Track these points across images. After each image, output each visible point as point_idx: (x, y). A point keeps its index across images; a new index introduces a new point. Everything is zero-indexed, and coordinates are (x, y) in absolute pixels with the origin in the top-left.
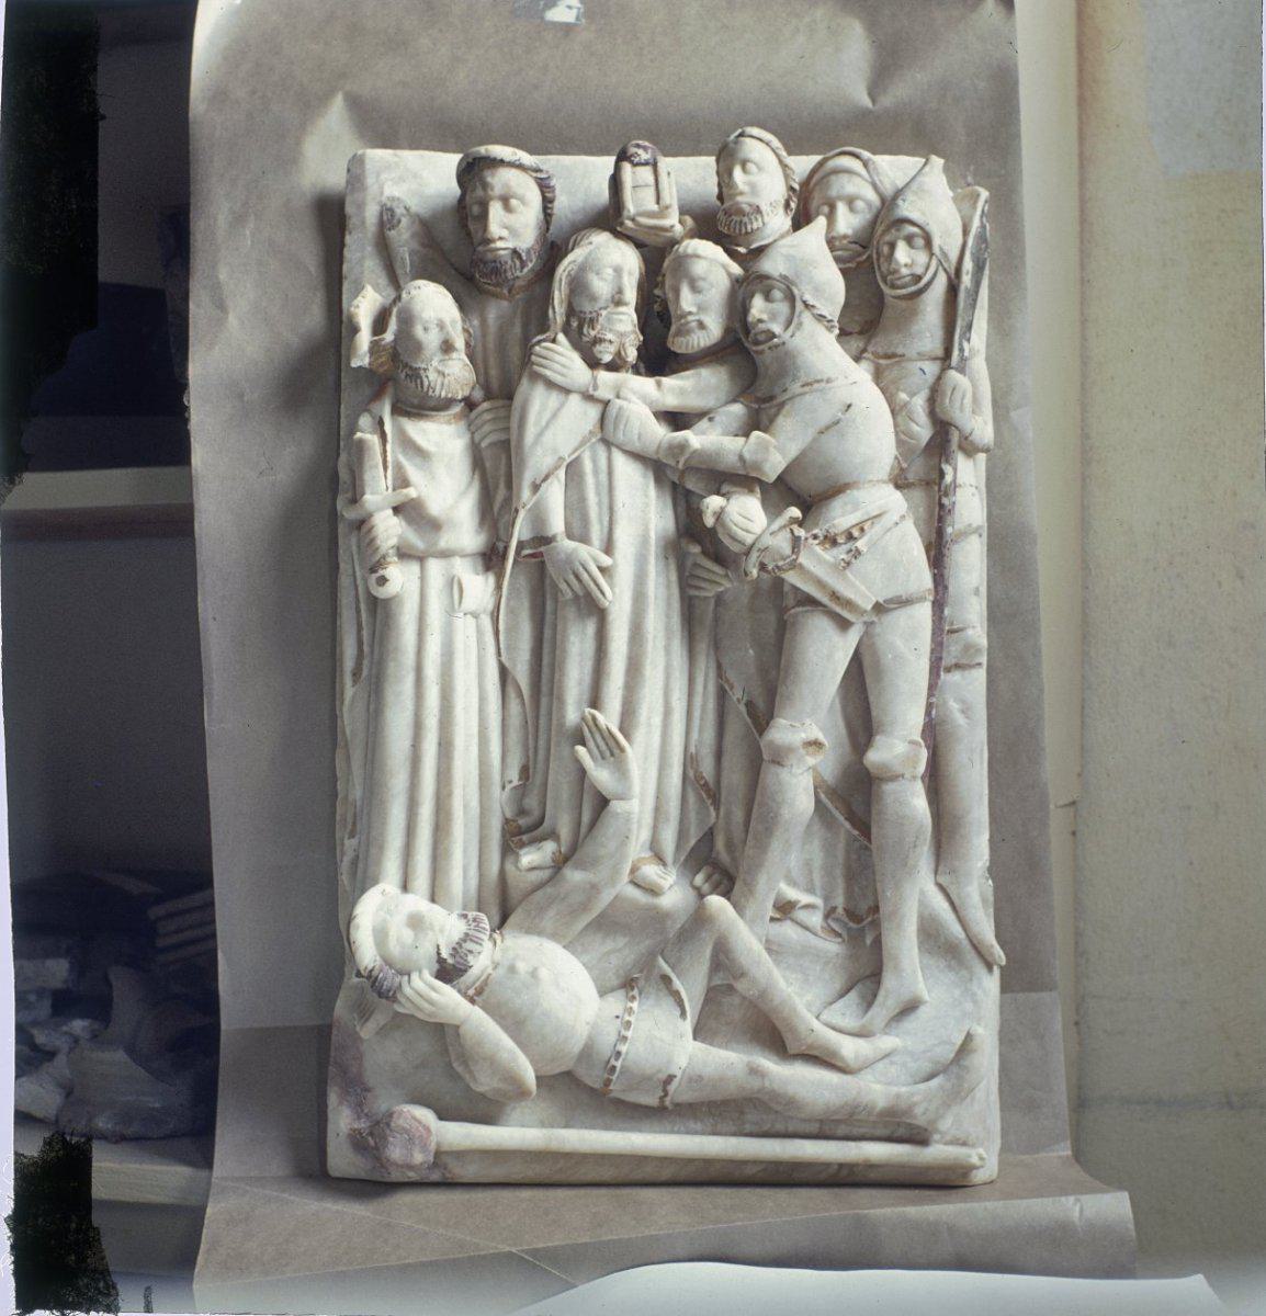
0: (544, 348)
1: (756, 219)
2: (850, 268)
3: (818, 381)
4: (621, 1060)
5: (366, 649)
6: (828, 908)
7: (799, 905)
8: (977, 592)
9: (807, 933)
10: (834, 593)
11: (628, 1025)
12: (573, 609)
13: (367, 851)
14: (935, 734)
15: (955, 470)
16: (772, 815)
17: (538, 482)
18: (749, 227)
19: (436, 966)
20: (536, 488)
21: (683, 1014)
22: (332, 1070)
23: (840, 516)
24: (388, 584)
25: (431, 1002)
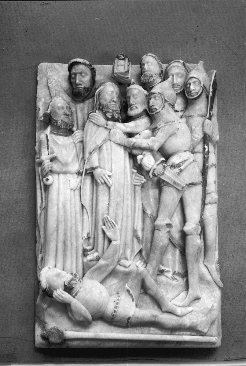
0: (93, 114)
1: (151, 78)
2: (178, 93)
3: (169, 122)
4: (115, 313)
5: (44, 200)
6: (173, 272)
7: (165, 270)
8: (200, 163)
9: (168, 278)
10: (174, 182)
11: (117, 303)
12: (65, 74)
13: (45, 257)
14: (202, 224)
15: (209, 147)
16: (157, 244)
17: (91, 152)
18: (149, 80)
19: (63, 288)
20: (90, 153)
21: (133, 300)
22: (36, 318)
23: (175, 160)
24: (49, 181)
25: (62, 297)
